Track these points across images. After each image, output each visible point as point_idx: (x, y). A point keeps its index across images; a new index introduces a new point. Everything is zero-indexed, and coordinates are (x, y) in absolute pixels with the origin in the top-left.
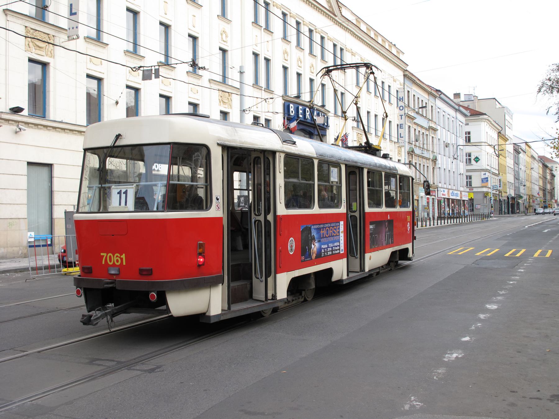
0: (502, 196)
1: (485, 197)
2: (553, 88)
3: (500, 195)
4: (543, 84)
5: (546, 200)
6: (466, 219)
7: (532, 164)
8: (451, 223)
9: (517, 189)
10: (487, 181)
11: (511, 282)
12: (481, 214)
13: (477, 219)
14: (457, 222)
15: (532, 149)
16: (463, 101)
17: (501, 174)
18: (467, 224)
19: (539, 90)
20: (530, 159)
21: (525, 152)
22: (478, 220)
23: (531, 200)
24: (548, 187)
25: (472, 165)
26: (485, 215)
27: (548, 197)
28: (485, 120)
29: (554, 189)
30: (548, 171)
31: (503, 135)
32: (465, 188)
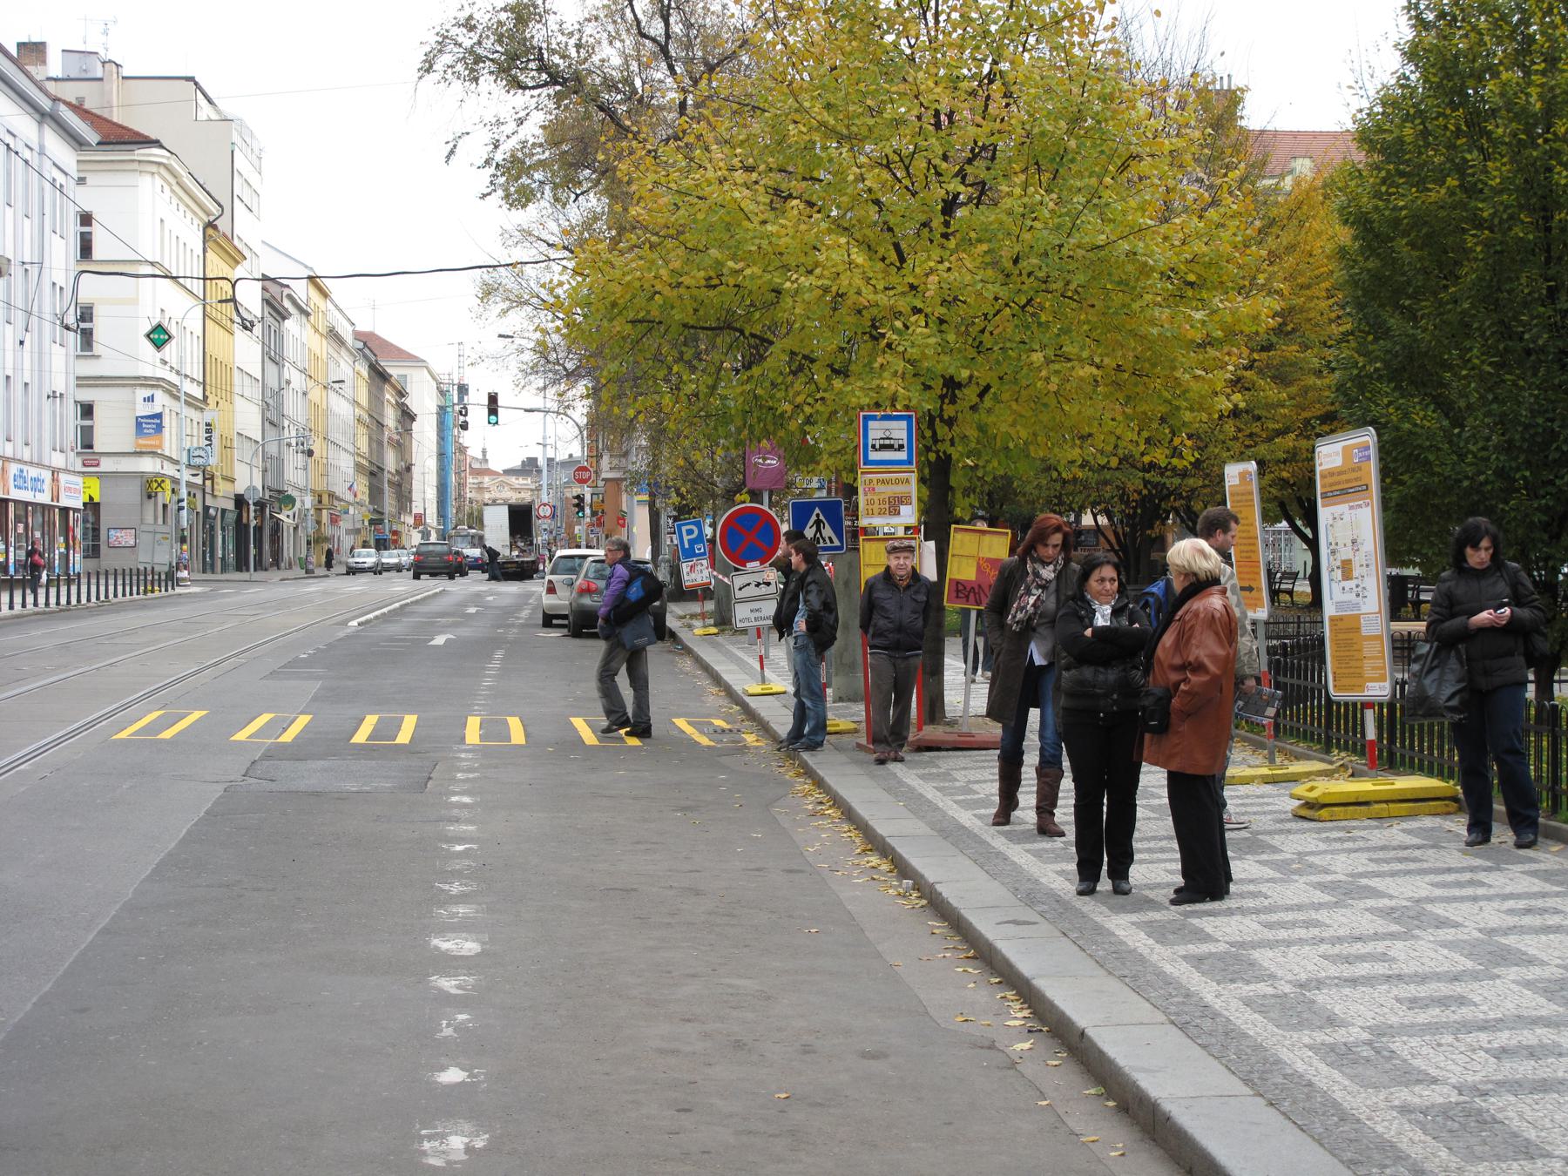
0: (214, 496)
1: (150, 497)
2: (479, 59)
3: (208, 490)
4: (444, 40)
5: (382, 514)
6: (74, 589)
7: (332, 365)
8: (24, 605)
9: (272, 465)
10: (159, 428)
11: (459, 848)
12: (142, 568)
13: (120, 589)
14: (47, 604)
15: (332, 301)
16: (56, 80)
17: (211, 400)
18: (90, 612)
19: (425, 61)
20: (324, 341)
21: (308, 314)
22: (131, 594)
23: (324, 512)
24: (391, 461)
25: (98, 357)
26: (160, 575)
27: (389, 503)
28: (154, 169)
29: (409, 469)
30: (389, 396)
31: (224, 235)
32: (72, 455)
